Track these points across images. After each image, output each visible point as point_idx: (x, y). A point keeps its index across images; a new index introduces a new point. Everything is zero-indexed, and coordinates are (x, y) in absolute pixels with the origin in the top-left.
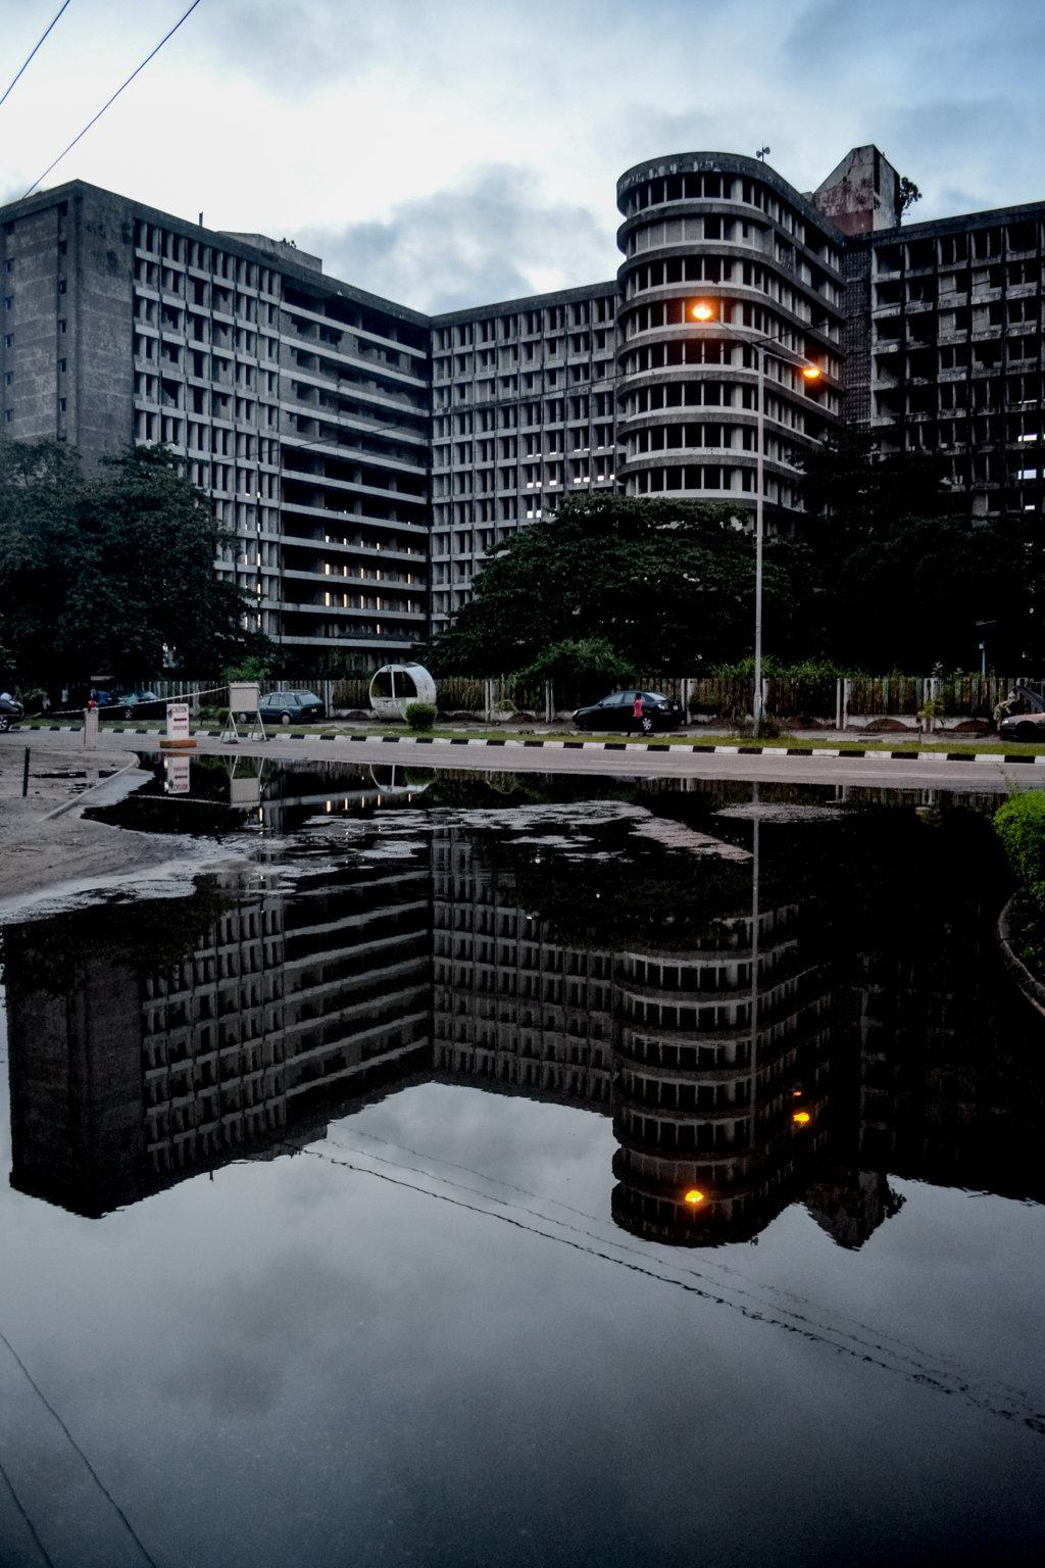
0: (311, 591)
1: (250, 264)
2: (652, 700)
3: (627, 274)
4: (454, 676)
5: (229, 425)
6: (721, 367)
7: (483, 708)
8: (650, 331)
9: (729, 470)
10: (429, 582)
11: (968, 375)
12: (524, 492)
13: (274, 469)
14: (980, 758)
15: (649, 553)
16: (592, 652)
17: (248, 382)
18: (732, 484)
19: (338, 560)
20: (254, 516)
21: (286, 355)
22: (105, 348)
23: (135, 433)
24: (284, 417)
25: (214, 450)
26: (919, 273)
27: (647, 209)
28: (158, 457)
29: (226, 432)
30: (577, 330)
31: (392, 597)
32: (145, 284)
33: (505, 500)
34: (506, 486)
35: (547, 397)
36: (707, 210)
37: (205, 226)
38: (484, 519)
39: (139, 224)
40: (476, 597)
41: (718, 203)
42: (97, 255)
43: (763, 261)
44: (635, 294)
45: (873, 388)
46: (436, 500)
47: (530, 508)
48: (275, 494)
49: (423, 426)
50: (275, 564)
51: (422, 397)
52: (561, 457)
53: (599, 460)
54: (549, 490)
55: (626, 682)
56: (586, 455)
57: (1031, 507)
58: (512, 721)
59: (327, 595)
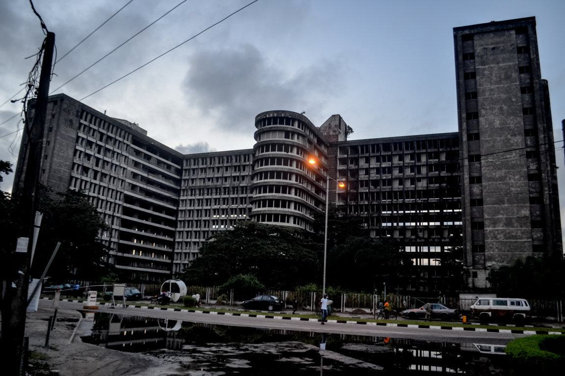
0: (129, 249)
1: (122, 130)
2: (273, 299)
3: (257, 147)
4: (194, 285)
5: (106, 185)
6: (288, 181)
7: (205, 299)
8: (264, 167)
9: (289, 216)
10: (174, 249)
11: (369, 191)
12: (212, 219)
13: (121, 203)
14: (454, 329)
15: (268, 244)
16: (250, 279)
17: (115, 171)
18: (290, 222)
19: (140, 238)
20: (111, 219)
21: (130, 162)
22: (63, 153)
23: (70, 184)
24: (127, 184)
25: (99, 194)
26: (353, 156)
27: (265, 127)
28: (80, 194)
29: (104, 187)
30: (236, 164)
31: (159, 253)
32: (82, 132)
33: (205, 221)
34: (206, 216)
35: (223, 186)
36: (286, 129)
37: (106, 114)
38: (197, 227)
39: (83, 111)
40: (200, 256)
41: (289, 127)
42: (66, 120)
43: (304, 148)
44: (259, 154)
45: (337, 192)
46: (179, 219)
47: (214, 224)
48: (120, 211)
49: (177, 192)
50: (116, 238)
51: (178, 182)
52: (227, 207)
53: (241, 209)
54: (221, 218)
55: (262, 292)
56: (236, 207)
57: (389, 236)
58: (216, 304)
59: (134, 251)
